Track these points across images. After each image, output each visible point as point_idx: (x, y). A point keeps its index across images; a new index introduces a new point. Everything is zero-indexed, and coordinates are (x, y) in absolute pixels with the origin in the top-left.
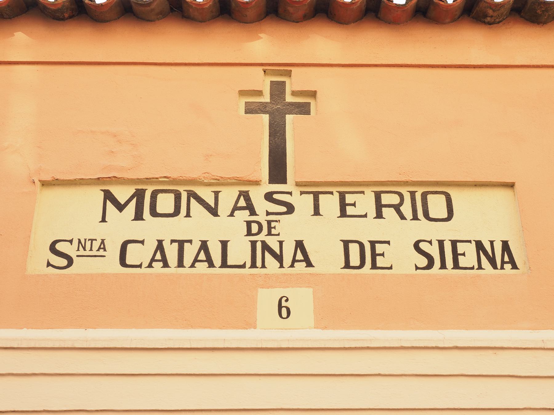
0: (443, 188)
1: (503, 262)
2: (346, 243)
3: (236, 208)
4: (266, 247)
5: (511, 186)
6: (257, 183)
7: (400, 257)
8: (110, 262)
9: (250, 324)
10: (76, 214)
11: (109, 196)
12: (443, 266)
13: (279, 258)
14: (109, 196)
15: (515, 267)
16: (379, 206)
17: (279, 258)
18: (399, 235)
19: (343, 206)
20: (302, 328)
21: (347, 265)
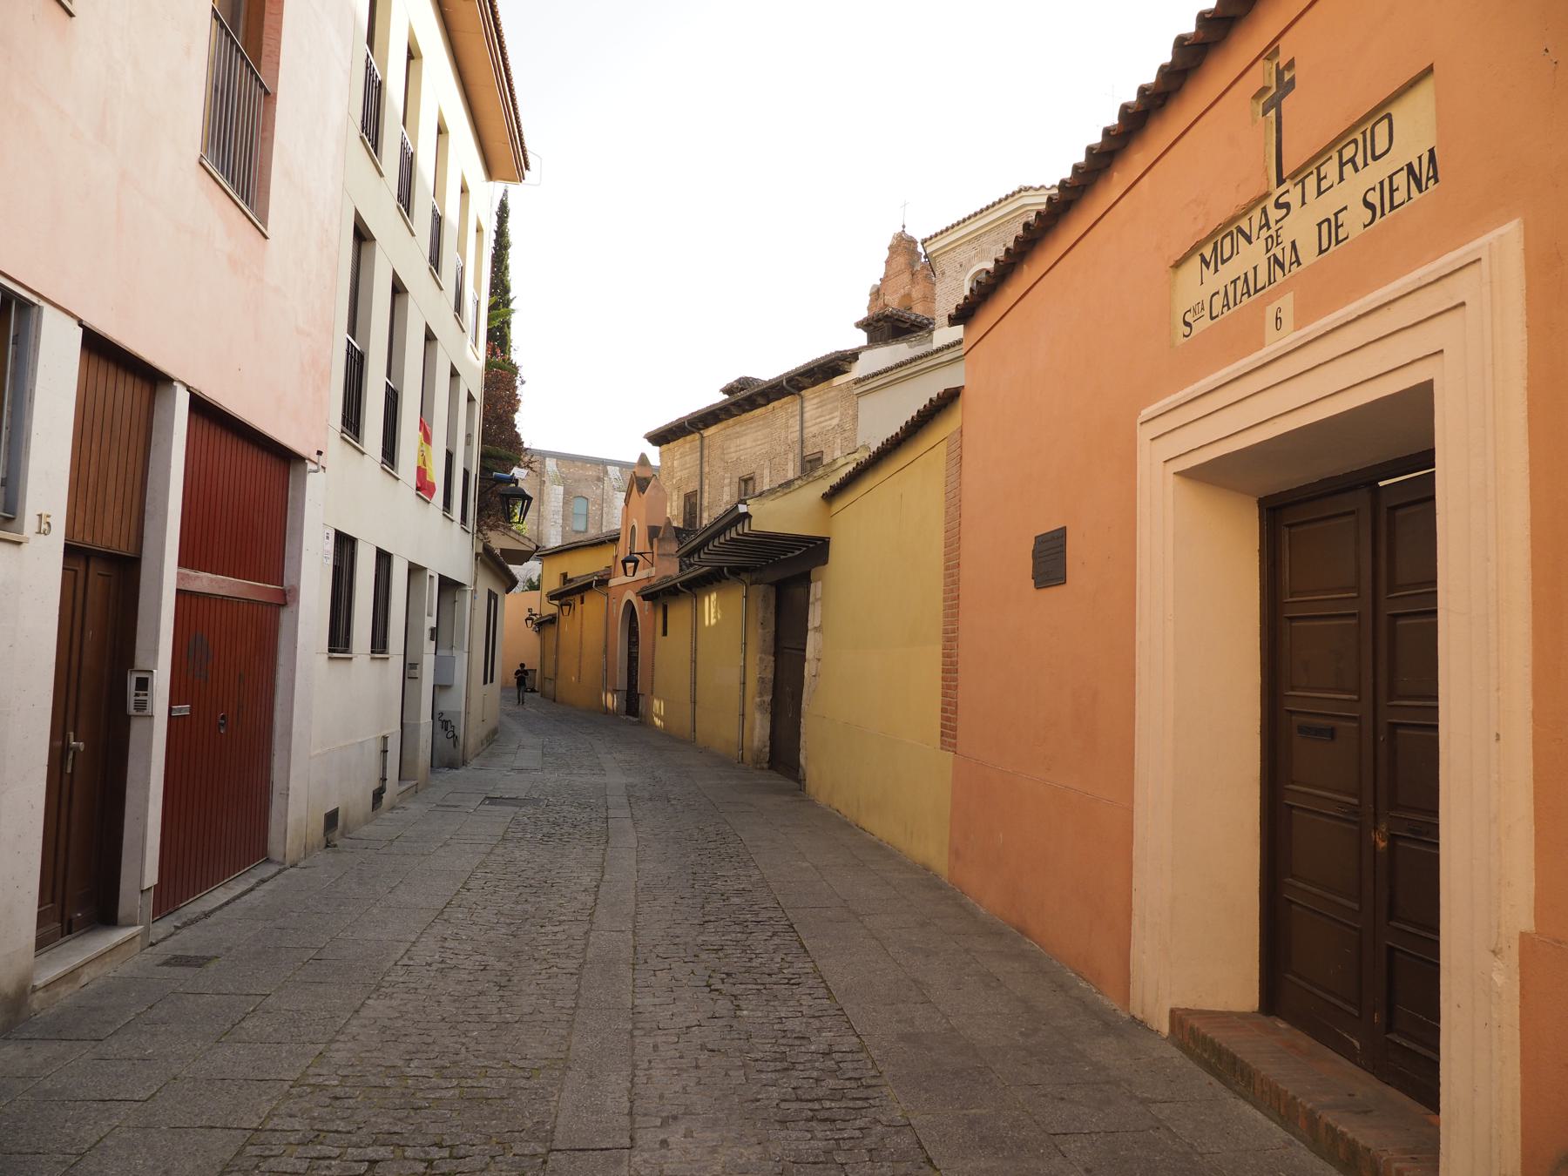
0: (1381, 111)
1: (1428, 179)
2: (1320, 225)
3: (1261, 228)
4: (1276, 260)
5: (1429, 70)
6: (1267, 195)
7: (1355, 219)
8: (1206, 322)
9: (1262, 345)
10: (1196, 286)
11: (1203, 259)
12: (1383, 214)
13: (1282, 266)
14: (1203, 259)
15: (1437, 181)
16: (1342, 165)
17: (1282, 266)
18: (1348, 192)
19: (1319, 180)
20: (1290, 338)
21: (1321, 252)
